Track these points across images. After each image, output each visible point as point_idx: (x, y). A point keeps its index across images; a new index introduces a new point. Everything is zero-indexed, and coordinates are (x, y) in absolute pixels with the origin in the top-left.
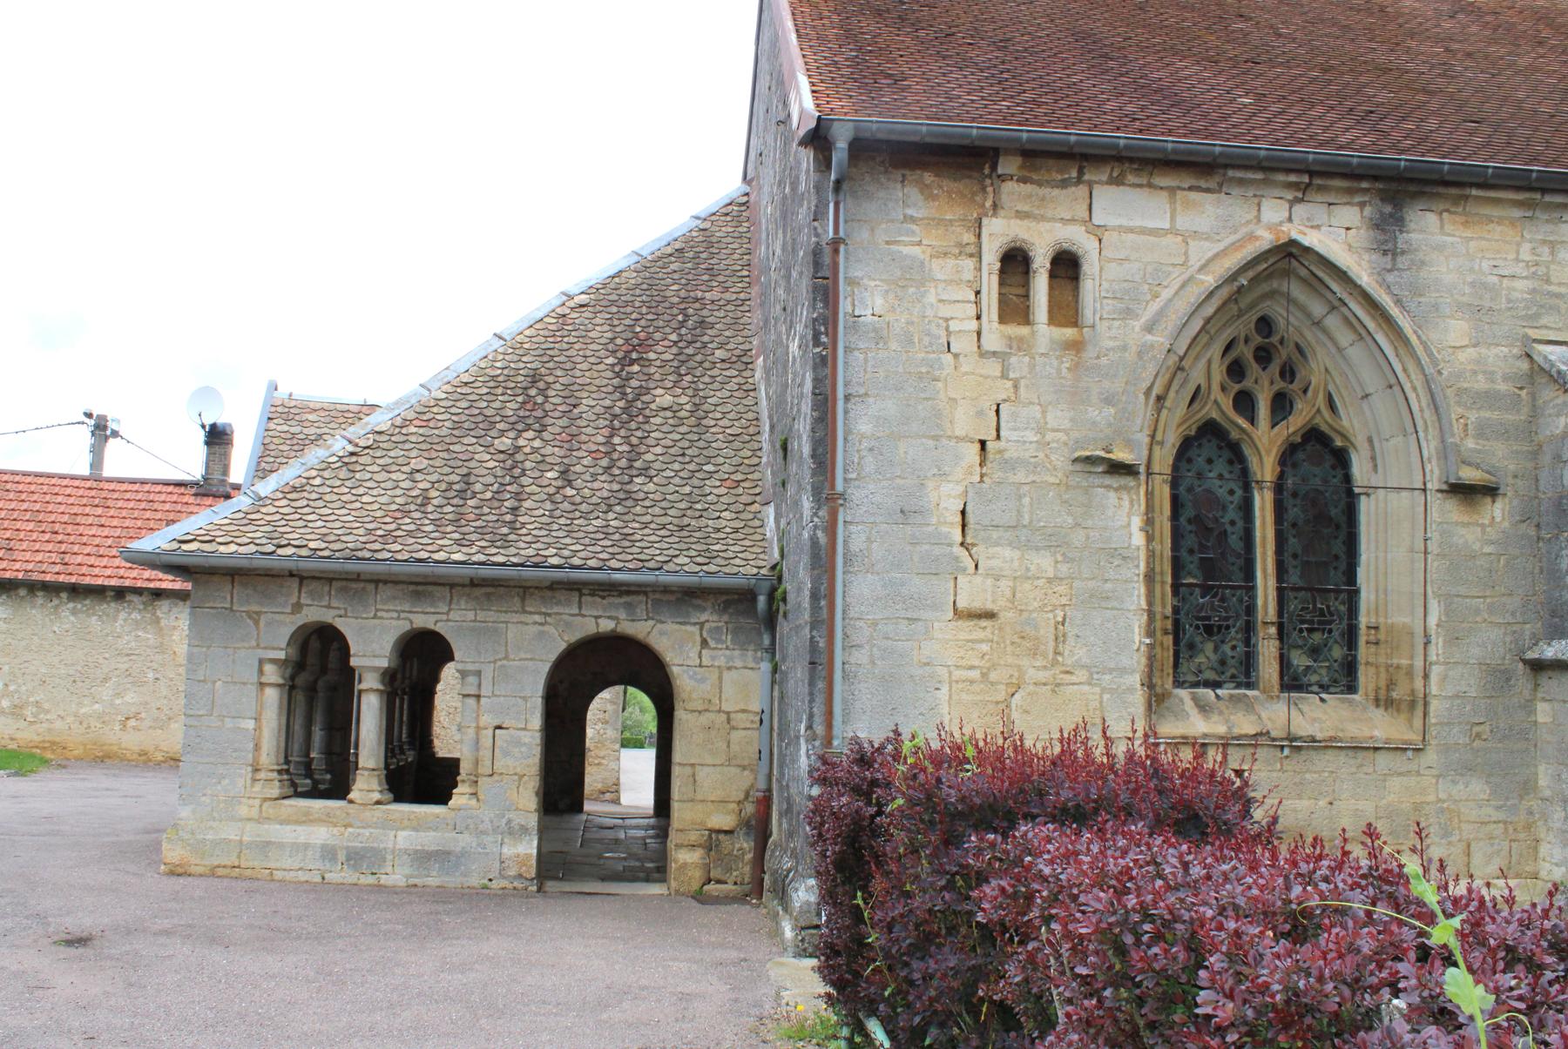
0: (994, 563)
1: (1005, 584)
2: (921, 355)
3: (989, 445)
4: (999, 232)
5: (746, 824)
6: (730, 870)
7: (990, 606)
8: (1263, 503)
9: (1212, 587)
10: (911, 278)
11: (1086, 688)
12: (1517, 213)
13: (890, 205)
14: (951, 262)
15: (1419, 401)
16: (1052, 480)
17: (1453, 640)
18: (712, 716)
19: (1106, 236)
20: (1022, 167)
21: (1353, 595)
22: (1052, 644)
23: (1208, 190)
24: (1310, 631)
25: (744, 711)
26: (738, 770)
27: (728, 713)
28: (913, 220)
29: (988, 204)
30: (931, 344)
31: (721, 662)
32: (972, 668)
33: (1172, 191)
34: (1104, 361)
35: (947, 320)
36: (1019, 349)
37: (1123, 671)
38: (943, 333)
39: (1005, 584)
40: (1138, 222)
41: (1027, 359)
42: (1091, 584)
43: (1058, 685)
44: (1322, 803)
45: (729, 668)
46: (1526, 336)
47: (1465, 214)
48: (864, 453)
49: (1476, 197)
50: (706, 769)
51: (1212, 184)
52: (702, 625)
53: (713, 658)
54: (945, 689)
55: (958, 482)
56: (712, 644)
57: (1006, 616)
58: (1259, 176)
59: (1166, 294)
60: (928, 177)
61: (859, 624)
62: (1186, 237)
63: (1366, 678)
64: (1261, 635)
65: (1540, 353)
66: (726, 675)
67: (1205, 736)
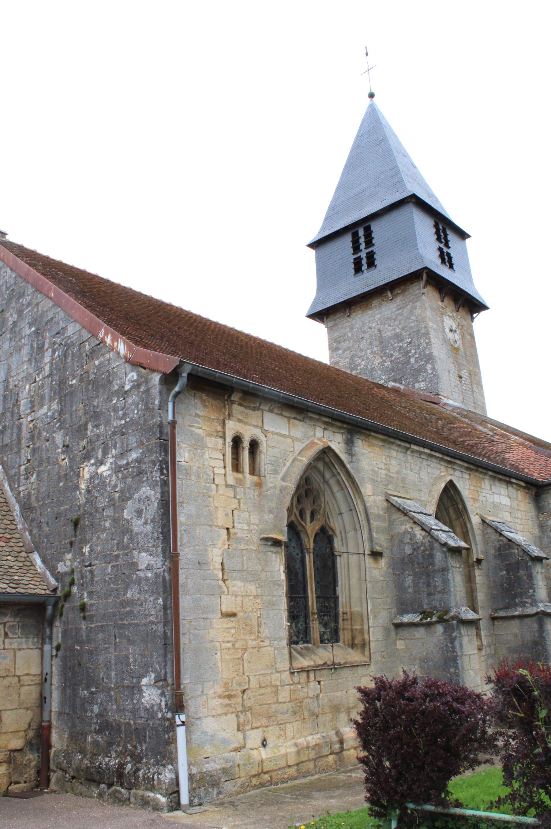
0: (235, 589)
1: (239, 599)
2: (204, 484)
3: (231, 530)
4: (232, 427)
5: (29, 744)
6: (21, 774)
7: (234, 610)
8: (309, 559)
9: (294, 597)
10: (198, 445)
11: (269, 648)
12: (381, 444)
13: (190, 407)
14: (214, 439)
15: (362, 517)
16: (253, 548)
17: (375, 617)
18: (9, 679)
19: (268, 435)
20: (240, 398)
21: (337, 598)
22: (257, 628)
23: (299, 420)
24: (324, 615)
25: (28, 675)
26: (25, 711)
27: (19, 677)
28: (197, 415)
29: (227, 413)
30: (207, 479)
31: (15, 646)
32: (229, 642)
33: (289, 418)
34: (269, 493)
35: (213, 467)
36: (240, 485)
37: (281, 639)
38: (212, 474)
39: (239, 599)
40: (278, 431)
41: (243, 490)
42: (268, 598)
43: (260, 648)
44: (344, 692)
45: (20, 649)
46: (386, 492)
47: (368, 442)
48: (183, 532)
49: (374, 436)
50: (8, 713)
51: (301, 418)
52: (5, 624)
53: (11, 644)
54: (219, 654)
55: (220, 548)
56: (10, 635)
57: (240, 615)
58: (317, 417)
59: (288, 464)
60: (204, 397)
61: (184, 622)
62: (294, 439)
63: (344, 635)
64: (311, 618)
65: (394, 500)
66: (19, 654)
67: (308, 666)
